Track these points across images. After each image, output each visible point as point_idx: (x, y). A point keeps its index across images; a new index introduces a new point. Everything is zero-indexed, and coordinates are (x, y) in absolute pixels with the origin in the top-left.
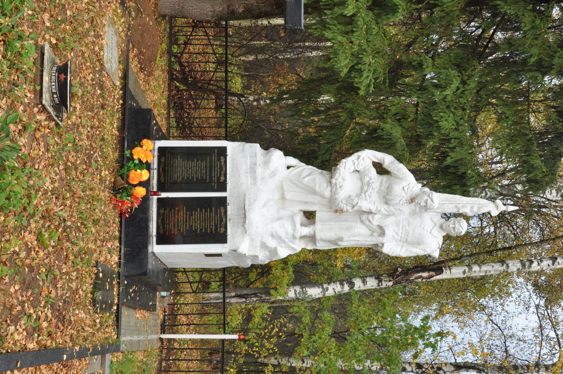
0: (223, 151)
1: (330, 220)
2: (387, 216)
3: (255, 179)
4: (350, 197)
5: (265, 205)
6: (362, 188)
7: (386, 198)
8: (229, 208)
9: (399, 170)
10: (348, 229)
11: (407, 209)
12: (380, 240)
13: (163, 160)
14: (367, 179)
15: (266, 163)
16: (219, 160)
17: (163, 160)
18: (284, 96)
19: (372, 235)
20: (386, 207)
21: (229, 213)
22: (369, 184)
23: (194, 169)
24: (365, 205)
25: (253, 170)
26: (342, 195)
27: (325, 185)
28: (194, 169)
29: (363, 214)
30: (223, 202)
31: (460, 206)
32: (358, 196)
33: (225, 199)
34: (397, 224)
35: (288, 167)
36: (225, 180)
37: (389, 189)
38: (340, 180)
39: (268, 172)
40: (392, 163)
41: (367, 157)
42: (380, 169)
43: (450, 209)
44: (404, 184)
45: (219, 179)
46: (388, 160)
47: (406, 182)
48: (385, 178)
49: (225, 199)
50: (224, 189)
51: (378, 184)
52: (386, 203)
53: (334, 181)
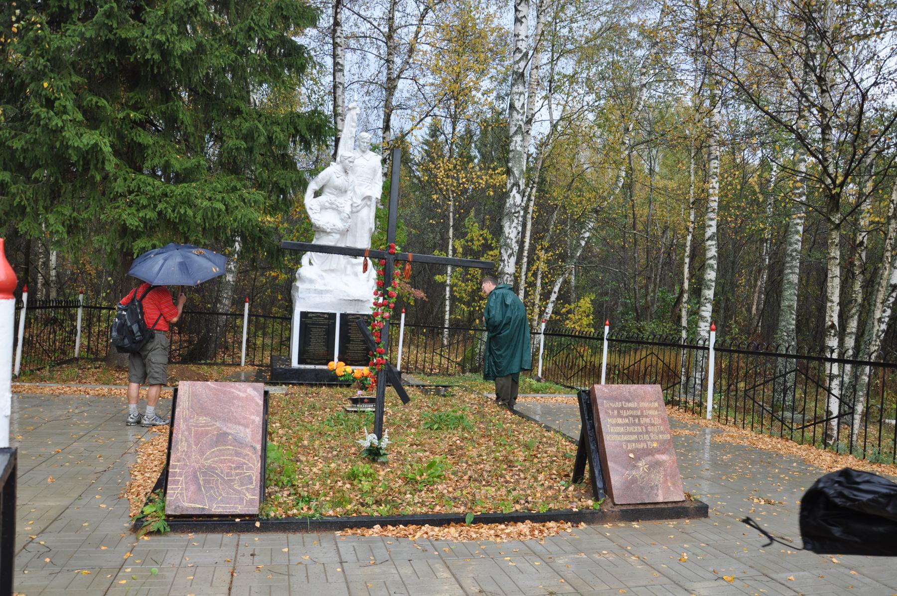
0: (304, 315)
1: (355, 236)
2: (355, 192)
3: (327, 291)
4: (342, 220)
5: (346, 284)
6: (333, 209)
7: (342, 191)
8: (348, 312)
9: (323, 179)
10: (363, 223)
11: (351, 177)
12: (374, 200)
13: (309, 361)
14: (327, 204)
15: (311, 281)
16: (311, 318)
17: (309, 361)
18: (607, 329)
19: (369, 206)
20: (349, 192)
21: (352, 312)
22: (331, 204)
23: (317, 336)
24: (348, 209)
25: (320, 292)
26: (340, 225)
27: (330, 237)
28: (317, 336)
29: (355, 211)
30: (344, 316)
31: (350, 136)
32: (340, 212)
33: (342, 315)
34: (361, 185)
35: (310, 263)
36: (327, 314)
37: (336, 188)
38: (328, 225)
39: (319, 280)
40: (316, 183)
41: (309, 200)
42: (317, 194)
43: (351, 143)
44: (334, 176)
45: (326, 319)
46: (313, 186)
47: (332, 172)
48: (326, 190)
49: (342, 315)
50: (335, 314)
51: (332, 196)
52: (346, 192)
53: (328, 230)
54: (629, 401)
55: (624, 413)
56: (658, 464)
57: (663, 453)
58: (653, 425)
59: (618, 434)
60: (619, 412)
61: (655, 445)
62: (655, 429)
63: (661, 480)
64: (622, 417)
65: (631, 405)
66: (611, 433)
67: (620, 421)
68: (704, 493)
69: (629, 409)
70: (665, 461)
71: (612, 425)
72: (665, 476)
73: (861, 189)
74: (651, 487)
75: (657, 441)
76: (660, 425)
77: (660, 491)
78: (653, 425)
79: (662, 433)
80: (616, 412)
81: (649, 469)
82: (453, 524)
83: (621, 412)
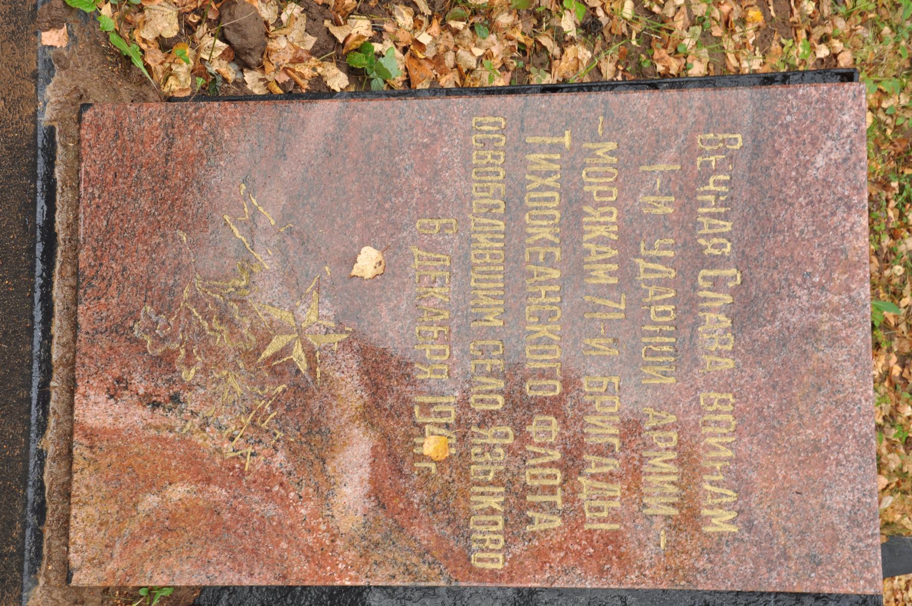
54: (746, 312)
55: (656, 264)
56: (314, 443)
57: (378, 494)
58: (572, 463)
59: (514, 204)
60: (661, 225)
61: (433, 445)
62: (543, 473)
63: (206, 441)
64: (627, 243)
65: (715, 324)
66: (518, 150)
67: (601, 225)
68: (347, 34)
69: (689, 306)
70: (325, 493)
71: (572, 166)
72: (234, 473)
73: (372, 40)
74: (165, 362)
75: (459, 463)
76: (573, 514)
77: (139, 415)
78: (572, 463)
79: (517, 514)
80: (664, 206)
81: (279, 367)
82: (384, 97)
83: (664, 247)
